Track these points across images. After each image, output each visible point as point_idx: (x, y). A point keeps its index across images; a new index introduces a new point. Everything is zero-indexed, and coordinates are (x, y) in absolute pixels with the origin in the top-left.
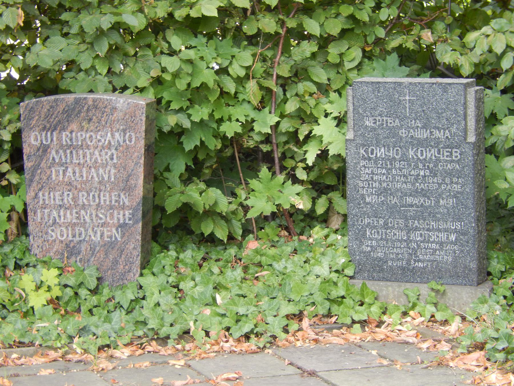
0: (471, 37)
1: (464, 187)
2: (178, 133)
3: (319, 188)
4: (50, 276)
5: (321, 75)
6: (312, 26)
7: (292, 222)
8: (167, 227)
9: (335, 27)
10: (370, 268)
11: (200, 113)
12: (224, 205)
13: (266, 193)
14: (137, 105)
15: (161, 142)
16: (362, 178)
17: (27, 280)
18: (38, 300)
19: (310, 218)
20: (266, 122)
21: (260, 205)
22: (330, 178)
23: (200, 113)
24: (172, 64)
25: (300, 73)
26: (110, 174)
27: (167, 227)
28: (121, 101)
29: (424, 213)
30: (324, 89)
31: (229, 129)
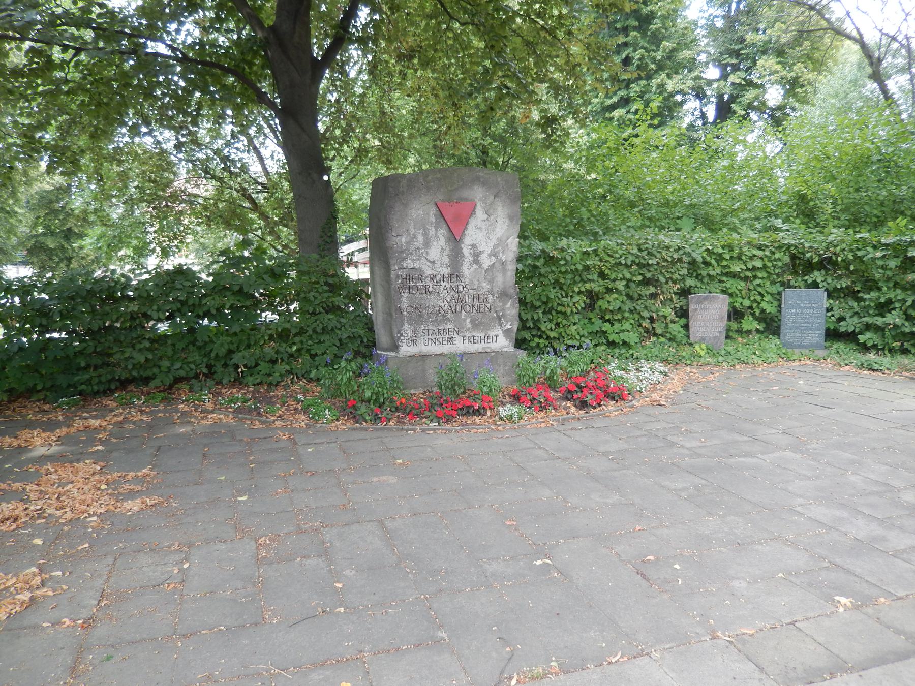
14: (414, 342)
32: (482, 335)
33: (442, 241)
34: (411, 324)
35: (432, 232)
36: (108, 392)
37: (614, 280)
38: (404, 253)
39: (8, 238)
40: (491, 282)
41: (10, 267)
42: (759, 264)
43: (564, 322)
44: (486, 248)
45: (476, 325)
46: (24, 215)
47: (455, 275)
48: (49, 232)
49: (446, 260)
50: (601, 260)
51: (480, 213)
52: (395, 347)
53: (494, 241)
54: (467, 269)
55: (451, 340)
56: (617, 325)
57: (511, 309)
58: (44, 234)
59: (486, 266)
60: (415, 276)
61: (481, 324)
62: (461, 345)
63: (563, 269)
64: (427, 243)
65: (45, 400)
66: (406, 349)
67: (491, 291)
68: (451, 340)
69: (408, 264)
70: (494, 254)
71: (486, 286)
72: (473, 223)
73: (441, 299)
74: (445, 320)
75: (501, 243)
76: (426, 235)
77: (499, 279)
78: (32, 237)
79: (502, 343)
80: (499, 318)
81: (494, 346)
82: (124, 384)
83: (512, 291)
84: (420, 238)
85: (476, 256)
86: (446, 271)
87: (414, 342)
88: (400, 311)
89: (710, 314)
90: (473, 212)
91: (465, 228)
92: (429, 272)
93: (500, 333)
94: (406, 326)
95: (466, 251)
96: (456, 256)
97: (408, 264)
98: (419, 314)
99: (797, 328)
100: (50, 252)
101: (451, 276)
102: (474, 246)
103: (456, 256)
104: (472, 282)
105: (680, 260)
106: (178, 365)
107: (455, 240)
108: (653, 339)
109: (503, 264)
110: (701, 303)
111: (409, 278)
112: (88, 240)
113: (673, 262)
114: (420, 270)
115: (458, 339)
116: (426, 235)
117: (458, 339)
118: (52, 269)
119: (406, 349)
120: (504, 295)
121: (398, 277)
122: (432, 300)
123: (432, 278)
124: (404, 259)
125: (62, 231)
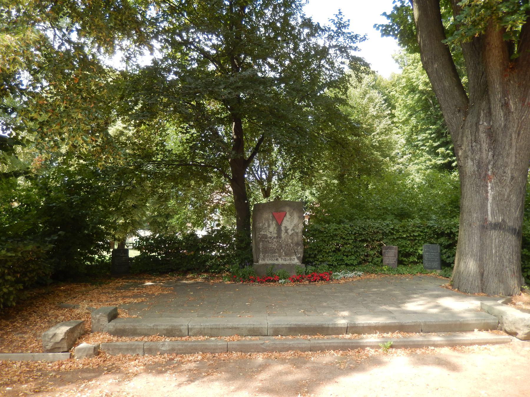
0: (441, 341)
1: (438, 258)
2: (401, 251)
3: (418, 259)
4: (386, 267)
5: (419, 244)
6: (417, 238)
7: (415, 263)
8: (400, 262)
9: (420, 238)
10: (426, 268)
11: (403, 249)
12: (406, 260)
13: (411, 259)
14: (264, 259)
15: (399, 252)
16: (425, 257)
17: (384, 267)
18: (385, 269)
19: (417, 263)
20: (411, 250)
21: (411, 260)
22: (420, 257)
23: (403, 249)
24: (400, 243)
25: (416, 244)
26: (393, 255)
27: (400, 262)
28: (395, 247)
29: (434, 261)
30: (419, 246)
31: (407, 251)
32: (289, 258)
33: (274, 225)
34: (263, 253)
35: (271, 222)
36: (167, 273)
37: (348, 240)
38: (261, 229)
39: (142, 217)
40: (292, 239)
41: (141, 231)
42: (416, 234)
43: (326, 255)
44: (290, 227)
45: (286, 255)
46: (149, 207)
47: (279, 236)
48: (160, 215)
49: (275, 232)
50: (342, 232)
51: (288, 216)
52: (257, 262)
53: (293, 225)
54: (283, 235)
55: (277, 260)
56: (349, 257)
57: (300, 249)
58: (157, 216)
59: (290, 234)
60: (265, 236)
61: (288, 254)
62: (281, 261)
63: (325, 235)
64: (269, 226)
65: (150, 274)
66: (261, 262)
67: (292, 243)
68: (277, 260)
69: (262, 233)
70: (293, 230)
71: (290, 241)
72: (285, 219)
73: (274, 246)
74: (275, 252)
75: (296, 226)
76: (268, 223)
77: (296, 238)
78: (152, 217)
79: (296, 261)
80: (295, 252)
81: (293, 262)
82: (172, 271)
83: (301, 243)
84: (267, 224)
85: (286, 230)
86: (275, 235)
87: (264, 259)
88: (259, 249)
89: (391, 255)
90: (285, 215)
91: (282, 221)
92: (269, 236)
93: (295, 258)
94: (261, 254)
95: (283, 229)
96: (279, 231)
97: (262, 233)
98: (266, 251)
99: (429, 261)
100: (159, 224)
101: (277, 237)
102: (286, 227)
103: (279, 231)
104: (285, 239)
105: (378, 232)
106: (189, 265)
107: (279, 225)
108: (367, 263)
109: (297, 233)
110: (387, 249)
111: (262, 237)
112: (174, 220)
113: (375, 233)
114: (266, 235)
115: (280, 259)
116: (268, 223)
117: (280, 259)
118: (159, 232)
119: (261, 262)
120: (297, 244)
121: (259, 237)
122: (270, 245)
123: (270, 238)
124: (261, 231)
125: (165, 214)
